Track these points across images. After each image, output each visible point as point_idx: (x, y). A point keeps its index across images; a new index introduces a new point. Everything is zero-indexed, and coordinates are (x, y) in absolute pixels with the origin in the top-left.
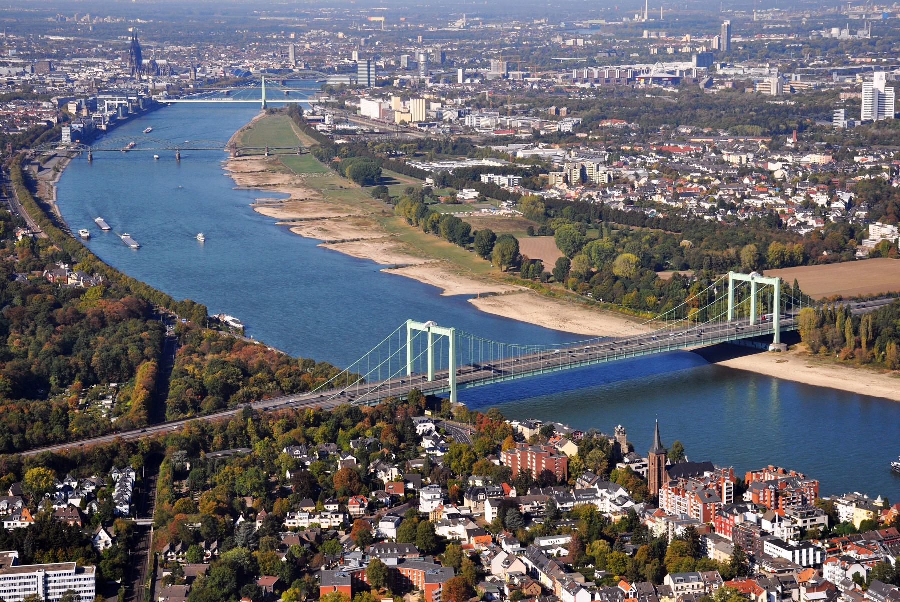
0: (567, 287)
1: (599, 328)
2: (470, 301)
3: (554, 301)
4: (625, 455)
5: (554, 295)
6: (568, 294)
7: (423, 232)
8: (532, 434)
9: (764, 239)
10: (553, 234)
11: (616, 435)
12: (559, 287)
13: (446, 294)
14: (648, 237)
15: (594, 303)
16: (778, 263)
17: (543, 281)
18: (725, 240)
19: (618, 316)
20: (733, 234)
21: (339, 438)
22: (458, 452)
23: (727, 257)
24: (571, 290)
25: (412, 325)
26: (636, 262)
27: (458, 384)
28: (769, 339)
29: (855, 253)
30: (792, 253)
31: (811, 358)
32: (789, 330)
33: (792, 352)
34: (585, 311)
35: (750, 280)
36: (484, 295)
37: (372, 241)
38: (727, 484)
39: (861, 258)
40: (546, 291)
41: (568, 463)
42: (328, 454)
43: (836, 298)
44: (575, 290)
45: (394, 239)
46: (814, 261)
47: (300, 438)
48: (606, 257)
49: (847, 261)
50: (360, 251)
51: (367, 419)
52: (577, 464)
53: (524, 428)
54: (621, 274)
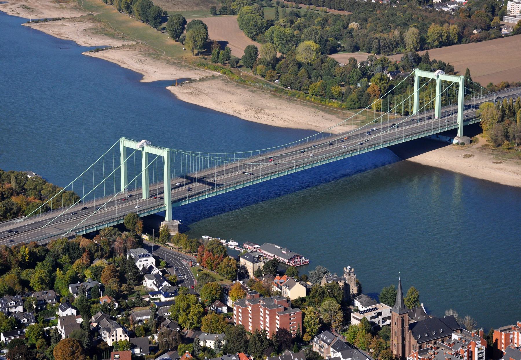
0: (255, 72)
1: (290, 118)
2: (168, 88)
3: (245, 88)
4: (354, 296)
5: (245, 81)
6: (257, 81)
7: (117, 11)
8: (256, 269)
9: (420, 18)
10: (233, 13)
11: (345, 276)
12: (249, 73)
13: (147, 80)
14: (319, 19)
15: (282, 91)
16: (436, 43)
17: (232, 67)
18: (387, 21)
19: (306, 105)
20: (392, 14)
21: (57, 280)
22: (186, 306)
23: (393, 40)
24: (259, 77)
25: (125, 143)
26: (317, 49)
27: (173, 202)
28: (453, 133)
29: (501, 30)
30: (448, 33)
31: (495, 152)
32: (470, 123)
33: (475, 146)
34: (275, 99)
35: (435, 78)
36: (180, 82)
37: (72, 20)
38: (478, 350)
39: (507, 35)
40: (237, 78)
41: (303, 317)
42: (46, 303)
43: (504, 85)
44: (263, 76)
45: (92, 18)
46: (467, 40)
47: (14, 284)
48: (287, 41)
49: (495, 38)
50: (62, 31)
51: (85, 255)
52: (312, 319)
53: (247, 261)
54: (303, 60)
